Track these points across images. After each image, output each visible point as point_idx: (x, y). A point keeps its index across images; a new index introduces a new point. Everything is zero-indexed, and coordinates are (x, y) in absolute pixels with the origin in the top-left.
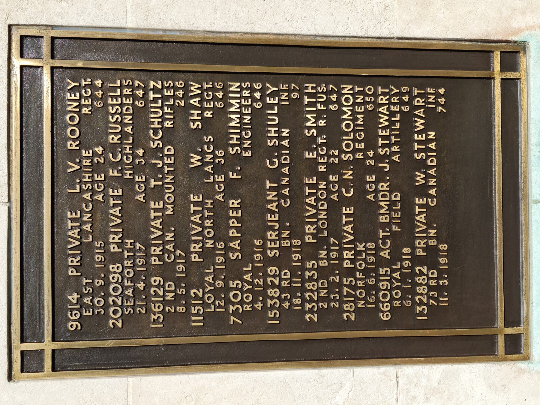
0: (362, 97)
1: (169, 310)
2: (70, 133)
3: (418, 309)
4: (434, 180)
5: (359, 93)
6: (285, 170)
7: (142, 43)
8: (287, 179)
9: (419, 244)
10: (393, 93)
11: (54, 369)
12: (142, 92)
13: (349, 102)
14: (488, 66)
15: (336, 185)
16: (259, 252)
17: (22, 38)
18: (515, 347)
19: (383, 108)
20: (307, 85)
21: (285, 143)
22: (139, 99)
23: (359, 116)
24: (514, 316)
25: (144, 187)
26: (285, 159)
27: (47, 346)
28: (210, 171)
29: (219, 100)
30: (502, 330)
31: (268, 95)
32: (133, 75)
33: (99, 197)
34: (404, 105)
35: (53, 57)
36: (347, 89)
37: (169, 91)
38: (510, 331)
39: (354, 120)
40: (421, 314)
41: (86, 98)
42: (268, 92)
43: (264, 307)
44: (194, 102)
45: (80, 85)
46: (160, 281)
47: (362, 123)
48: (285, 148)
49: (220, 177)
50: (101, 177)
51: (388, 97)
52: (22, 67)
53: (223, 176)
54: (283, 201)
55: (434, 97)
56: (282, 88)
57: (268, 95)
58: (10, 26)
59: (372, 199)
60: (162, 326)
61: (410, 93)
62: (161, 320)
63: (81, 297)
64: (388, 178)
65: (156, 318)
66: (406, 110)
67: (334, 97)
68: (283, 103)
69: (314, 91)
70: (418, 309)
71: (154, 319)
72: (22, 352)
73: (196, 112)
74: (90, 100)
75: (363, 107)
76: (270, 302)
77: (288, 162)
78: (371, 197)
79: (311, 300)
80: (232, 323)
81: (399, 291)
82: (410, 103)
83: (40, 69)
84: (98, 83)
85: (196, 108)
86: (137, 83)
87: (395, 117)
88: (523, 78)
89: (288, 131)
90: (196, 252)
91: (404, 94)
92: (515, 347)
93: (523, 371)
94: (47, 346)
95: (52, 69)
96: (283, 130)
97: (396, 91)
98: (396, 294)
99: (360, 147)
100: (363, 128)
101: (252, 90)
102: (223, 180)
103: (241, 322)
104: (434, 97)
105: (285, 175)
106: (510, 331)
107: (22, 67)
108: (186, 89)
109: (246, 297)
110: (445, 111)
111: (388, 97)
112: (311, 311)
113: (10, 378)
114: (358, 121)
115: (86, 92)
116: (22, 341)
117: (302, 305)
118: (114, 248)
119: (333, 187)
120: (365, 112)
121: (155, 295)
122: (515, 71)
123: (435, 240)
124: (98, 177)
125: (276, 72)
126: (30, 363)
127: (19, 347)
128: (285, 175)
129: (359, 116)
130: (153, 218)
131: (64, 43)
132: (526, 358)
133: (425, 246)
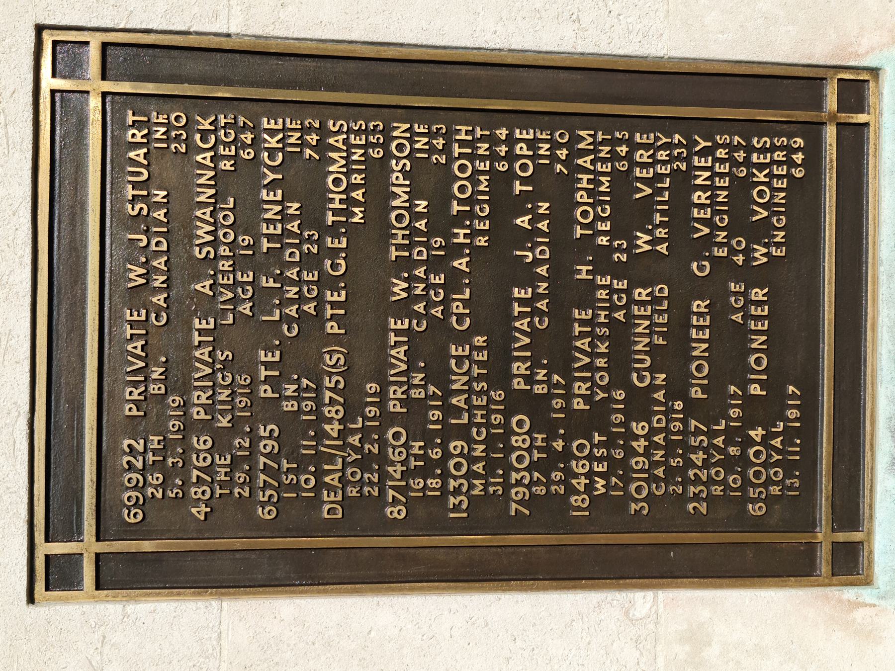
0: (487, 146)
1: (152, 493)
2: (581, 213)
3: (452, 500)
4: (546, 285)
5: (482, 139)
6: (542, 270)
7: (166, 51)
8: (546, 285)
9: (394, 393)
10: (659, 144)
11: (98, 588)
12: (742, 154)
13: (652, 160)
14: (818, 103)
15: (248, 288)
16: (372, 404)
17: (55, 43)
18: (850, 564)
19: (203, 156)
20: (458, 127)
21: (543, 225)
22: (739, 165)
23: (603, 179)
24: (851, 509)
25: (251, 291)
26: (542, 252)
27: (87, 546)
28: (463, 267)
29: (244, 146)
30: (824, 536)
31: (696, 153)
32: (327, 110)
33: (437, 312)
34: (619, 161)
35: (104, 77)
36: (400, 129)
37: (358, 138)
38: (58, 548)
39: (475, 183)
40: (457, 508)
41: (227, 145)
42: (697, 149)
43: (444, 488)
44: (585, 161)
45: (149, 120)
46: (273, 447)
47: (608, 190)
48: (543, 234)
49: (310, 275)
50: (248, 276)
51: (651, 152)
52: (53, 92)
53: (316, 273)
54: (538, 319)
55: (548, 146)
56: (290, 126)
57: (696, 153)
58: (40, 29)
59: (439, 315)
60: (465, 515)
61: (630, 142)
62: (464, 506)
63: (231, 471)
64: (467, 281)
65: (457, 503)
66: (798, 176)
67: (623, 150)
68: (418, 155)
69: (470, 138)
70: (452, 500)
71: (454, 504)
72: (47, 557)
73: (585, 177)
74: (233, 148)
75: (609, 164)
76: (514, 476)
77: (547, 256)
78: (738, 317)
79: (697, 480)
80: (513, 514)
81: (721, 469)
82: (629, 156)
83: (820, 127)
84: (502, 133)
85: (586, 171)
86: (241, 120)
87: (662, 182)
88: (878, 123)
89: (547, 205)
90: (580, 396)
91: (620, 142)
92: (850, 564)
93: (856, 605)
94: (87, 546)
95: (104, 95)
96: (417, 202)
97: (665, 140)
98: (776, 473)
99: (482, 227)
100: (608, 199)
101: (493, 141)
102: (316, 279)
103: (527, 512)
104: (548, 146)
105: (542, 279)
106: (58, 548)
107: (53, 92)
108: (386, 132)
109: (352, 474)
110: (566, 172)
111: (651, 152)
112: (696, 497)
113: (31, 599)
114: (479, 185)
115: (226, 135)
116: (47, 540)
117: (743, 488)
118: (265, 391)
119: (620, 299)
120: (492, 172)
121: (129, 469)
122: (862, 112)
123: (545, 386)
124: (242, 277)
125: (176, 93)
126: (54, 577)
127: (44, 549)
128: (542, 279)
129: (603, 179)
130: (196, 344)
131: (133, 55)
132: (868, 582)
133: (405, 396)
